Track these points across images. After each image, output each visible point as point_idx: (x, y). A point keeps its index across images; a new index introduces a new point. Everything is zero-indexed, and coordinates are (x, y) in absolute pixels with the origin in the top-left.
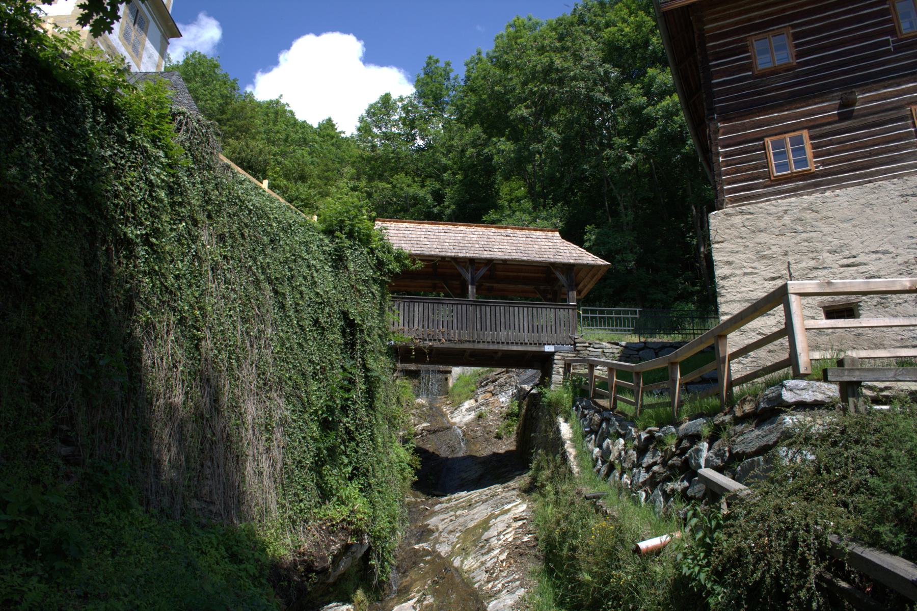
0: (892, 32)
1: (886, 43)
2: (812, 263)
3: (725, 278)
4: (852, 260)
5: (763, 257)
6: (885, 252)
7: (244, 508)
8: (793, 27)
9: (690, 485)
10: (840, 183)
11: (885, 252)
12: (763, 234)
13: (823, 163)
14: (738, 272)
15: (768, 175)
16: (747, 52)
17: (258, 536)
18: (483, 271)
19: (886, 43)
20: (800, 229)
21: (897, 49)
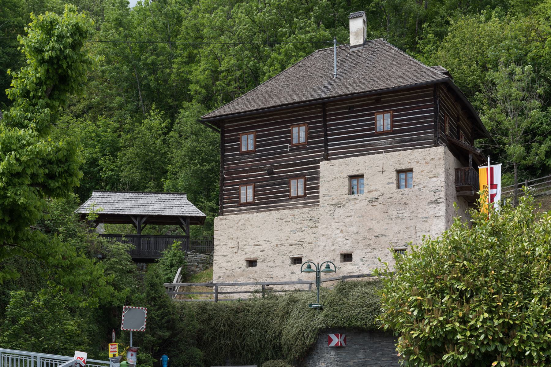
0: (290, 142)
1: (287, 147)
2: (245, 243)
3: (217, 246)
4: (258, 243)
5: (230, 239)
6: (268, 241)
7: (60, 155)
8: (257, 132)
9: (304, 196)
10: (260, 210)
11: (268, 241)
12: (231, 229)
13: (258, 199)
14: (222, 244)
15: (238, 202)
16: (239, 141)
17: (72, 171)
18: (144, 220)
19: (287, 147)
20: (243, 228)
21: (291, 151)
